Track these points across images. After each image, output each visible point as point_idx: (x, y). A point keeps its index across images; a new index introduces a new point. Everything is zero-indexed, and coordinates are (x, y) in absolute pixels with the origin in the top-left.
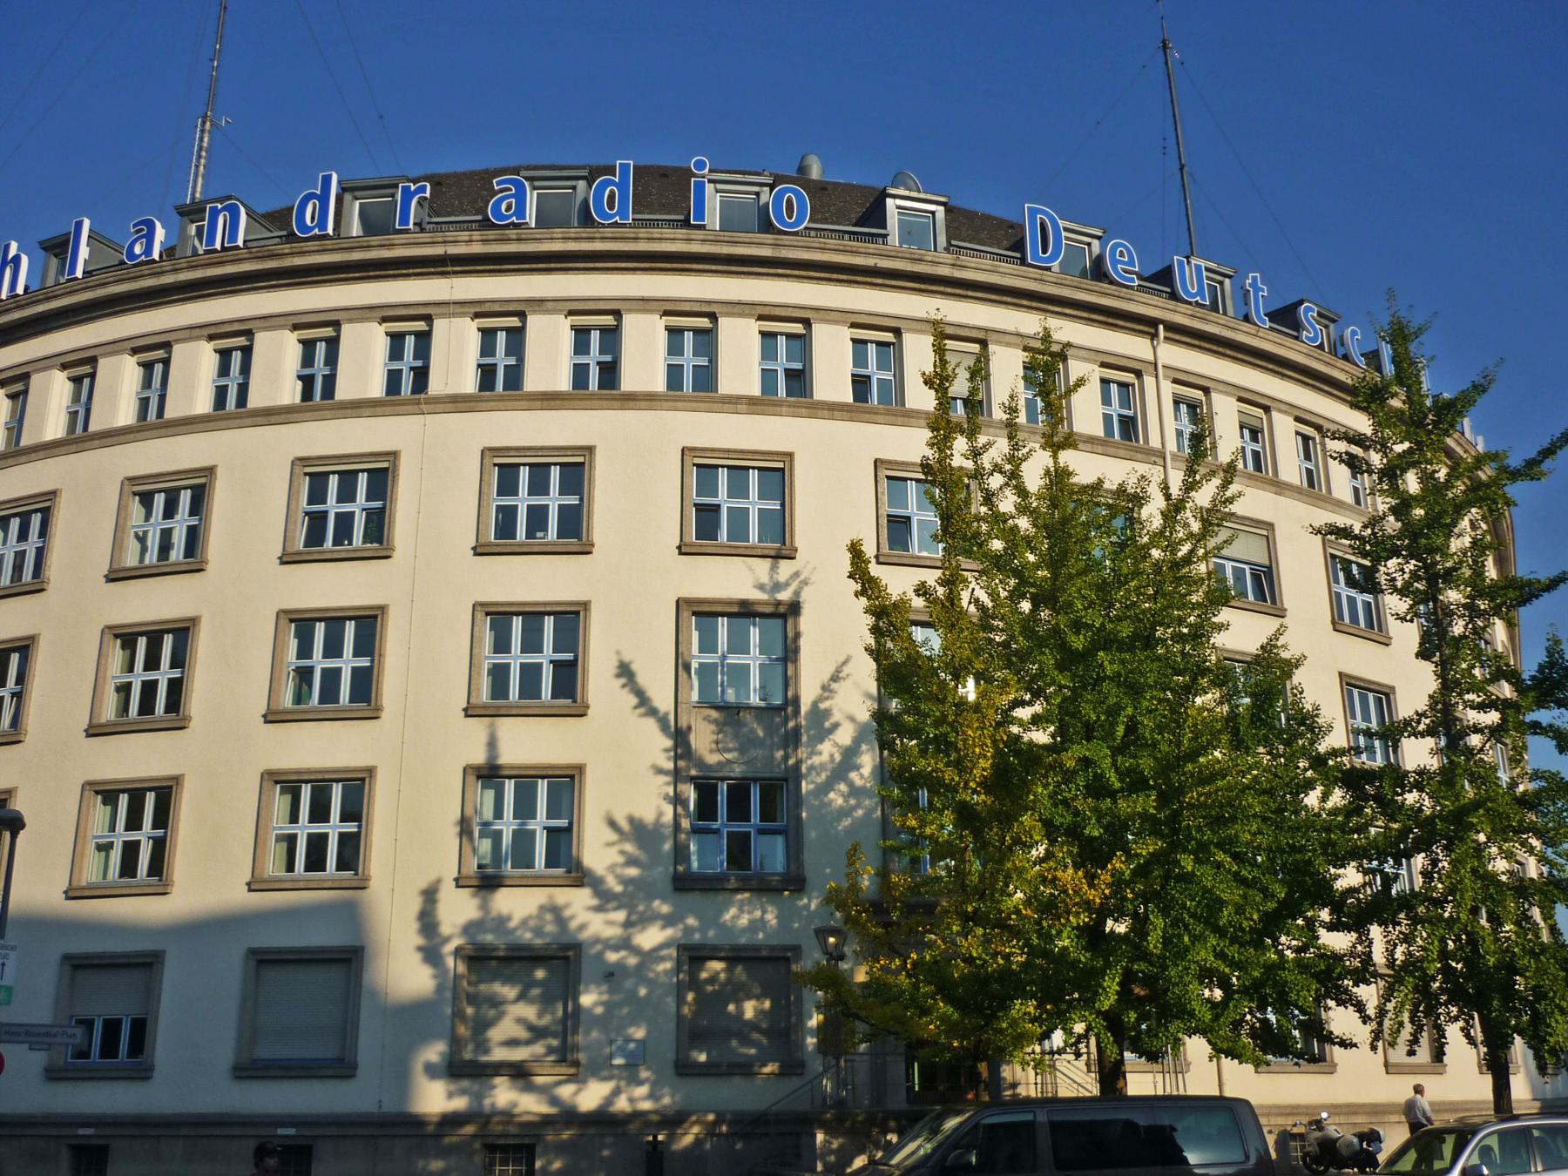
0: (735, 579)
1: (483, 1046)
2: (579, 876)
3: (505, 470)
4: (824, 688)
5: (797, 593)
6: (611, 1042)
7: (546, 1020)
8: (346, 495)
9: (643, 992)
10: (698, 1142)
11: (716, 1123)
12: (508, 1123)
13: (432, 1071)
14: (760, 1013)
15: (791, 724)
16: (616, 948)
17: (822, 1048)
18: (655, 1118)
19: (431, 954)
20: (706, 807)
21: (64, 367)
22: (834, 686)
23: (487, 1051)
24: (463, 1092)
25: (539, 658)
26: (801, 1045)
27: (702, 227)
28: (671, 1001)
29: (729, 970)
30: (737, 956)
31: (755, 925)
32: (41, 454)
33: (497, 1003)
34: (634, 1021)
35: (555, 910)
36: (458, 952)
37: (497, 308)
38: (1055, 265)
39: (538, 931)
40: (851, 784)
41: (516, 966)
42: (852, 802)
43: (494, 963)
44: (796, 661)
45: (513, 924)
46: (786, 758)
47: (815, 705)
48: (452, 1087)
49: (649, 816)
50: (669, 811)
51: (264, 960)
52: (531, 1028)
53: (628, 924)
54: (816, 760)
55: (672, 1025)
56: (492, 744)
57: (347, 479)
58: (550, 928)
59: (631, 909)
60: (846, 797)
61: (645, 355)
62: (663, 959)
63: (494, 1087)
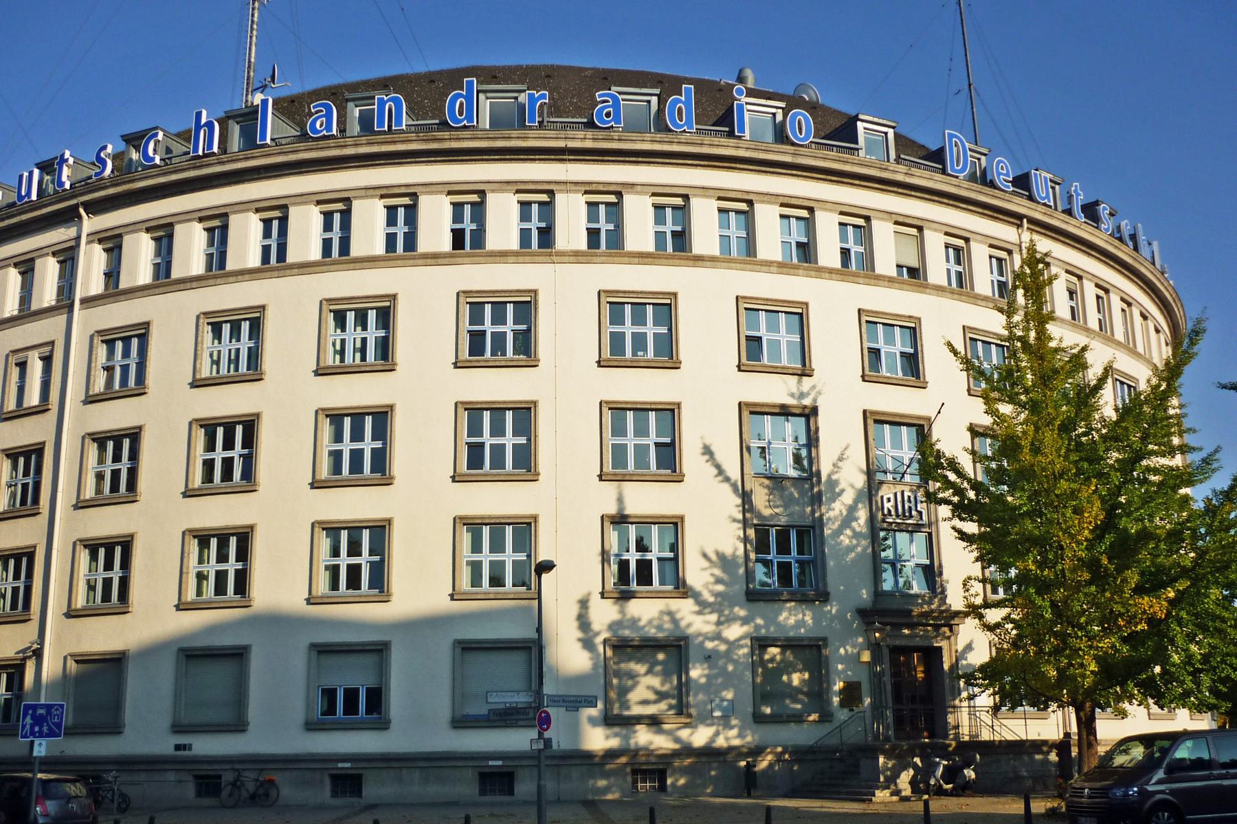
0: (777, 390)
1: (625, 705)
2: (682, 589)
3: (615, 306)
4: (834, 465)
5: (815, 400)
6: (711, 702)
7: (666, 688)
8: (499, 319)
9: (730, 668)
10: (771, 765)
11: (783, 753)
12: (648, 755)
13: (593, 721)
14: (803, 681)
15: (816, 490)
16: (712, 639)
17: (843, 704)
18: (745, 750)
19: (588, 644)
20: (762, 546)
21: (201, 220)
22: (840, 464)
23: (628, 708)
24: (616, 735)
25: (649, 442)
26: (829, 702)
27: (739, 138)
28: (748, 674)
29: (782, 653)
30: (789, 644)
31: (801, 624)
32: (247, 277)
33: (632, 676)
34: (726, 687)
35: (670, 614)
36: (605, 642)
37: (601, 188)
38: (961, 176)
39: (659, 628)
40: (853, 530)
41: (644, 651)
42: (855, 542)
43: (629, 650)
44: (817, 447)
45: (642, 623)
46: (813, 512)
47: (829, 476)
48: (608, 732)
49: (728, 551)
50: (741, 546)
51: (466, 648)
52: (657, 692)
53: (719, 623)
54: (831, 514)
55: (750, 689)
56: (620, 500)
57: (499, 308)
58: (667, 626)
59: (720, 613)
60: (850, 538)
61: (706, 229)
62: (742, 647)
63: (635, 732)
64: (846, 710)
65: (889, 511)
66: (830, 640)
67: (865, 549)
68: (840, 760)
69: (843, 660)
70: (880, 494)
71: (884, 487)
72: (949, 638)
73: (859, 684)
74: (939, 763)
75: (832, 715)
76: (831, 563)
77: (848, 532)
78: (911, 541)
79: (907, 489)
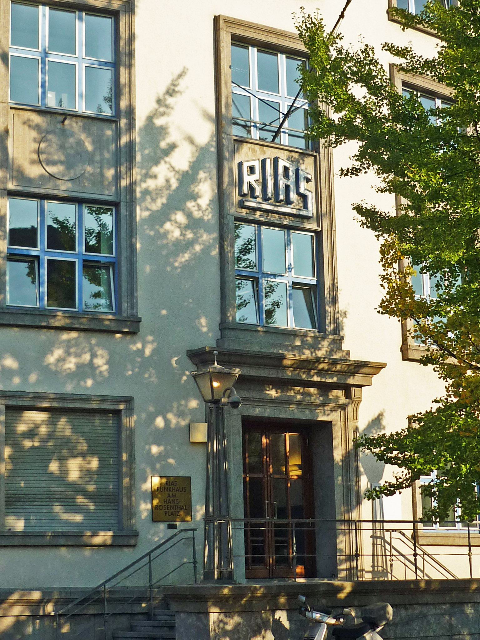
4: (159, 101)
14: (87, 473)
15: (124, 140)
22: (170, 100)
26: (132, 512)
29: (52, 422)
40: (189, 215)
42: (190, 235)
44: (130, 66)
46: (118, 177)
47: (150, 119)
54: (151, 184)
64: (162, 526)
65: (251, 188)
66: (138, 402)
67: (206, 250)
68: (147, 615)
69: (159, 437)
70: (238, 158)
71: (245, 148)
72: (343, 407)
73: (187, 480)
74: (319, 623)
75: (136, 535)
76: (145, 268)
77: (180, 217)
78: (287, 243)
79: (283, 155)
